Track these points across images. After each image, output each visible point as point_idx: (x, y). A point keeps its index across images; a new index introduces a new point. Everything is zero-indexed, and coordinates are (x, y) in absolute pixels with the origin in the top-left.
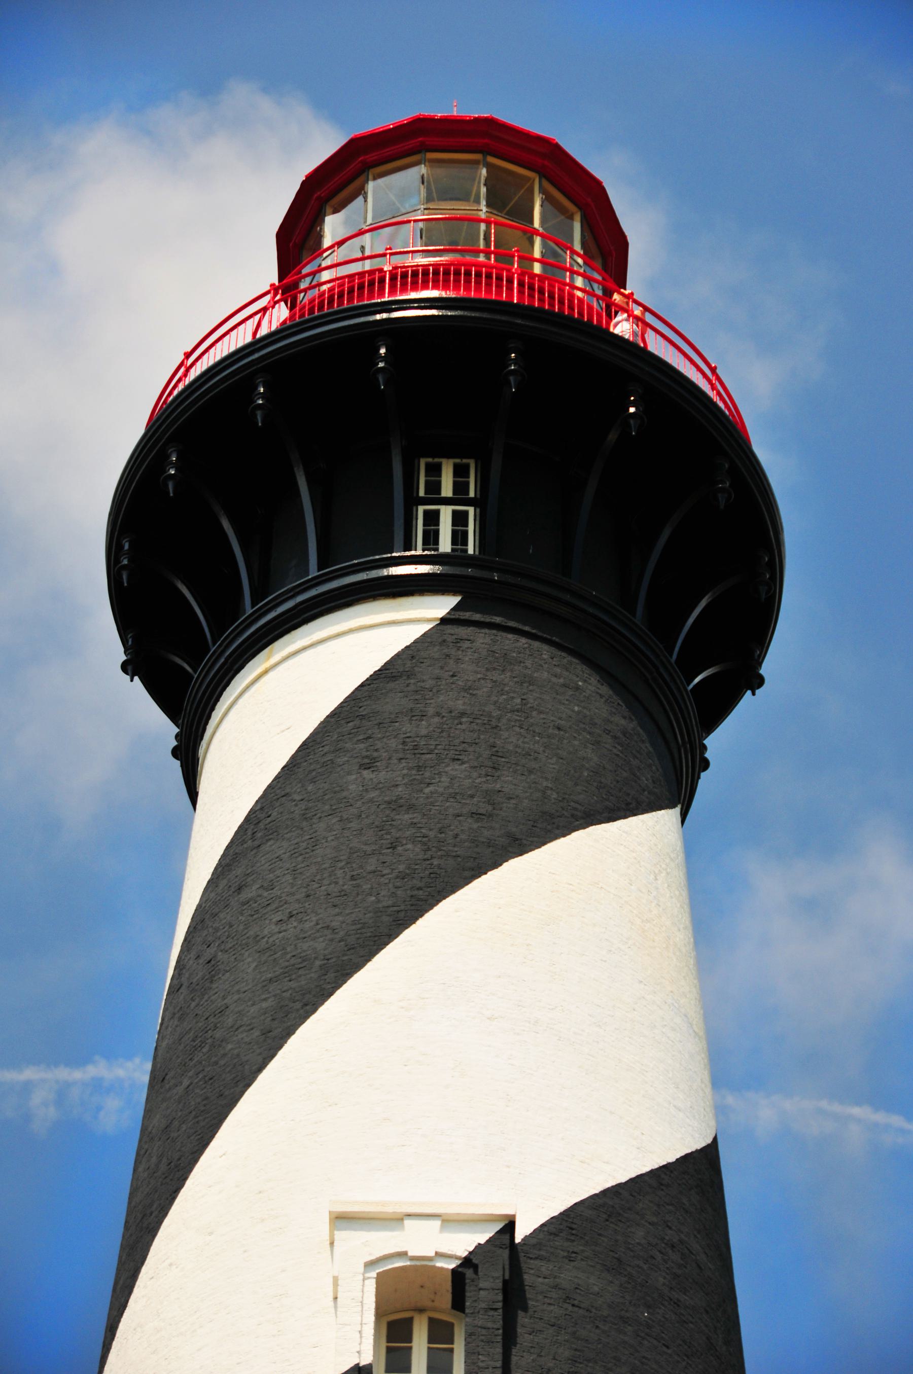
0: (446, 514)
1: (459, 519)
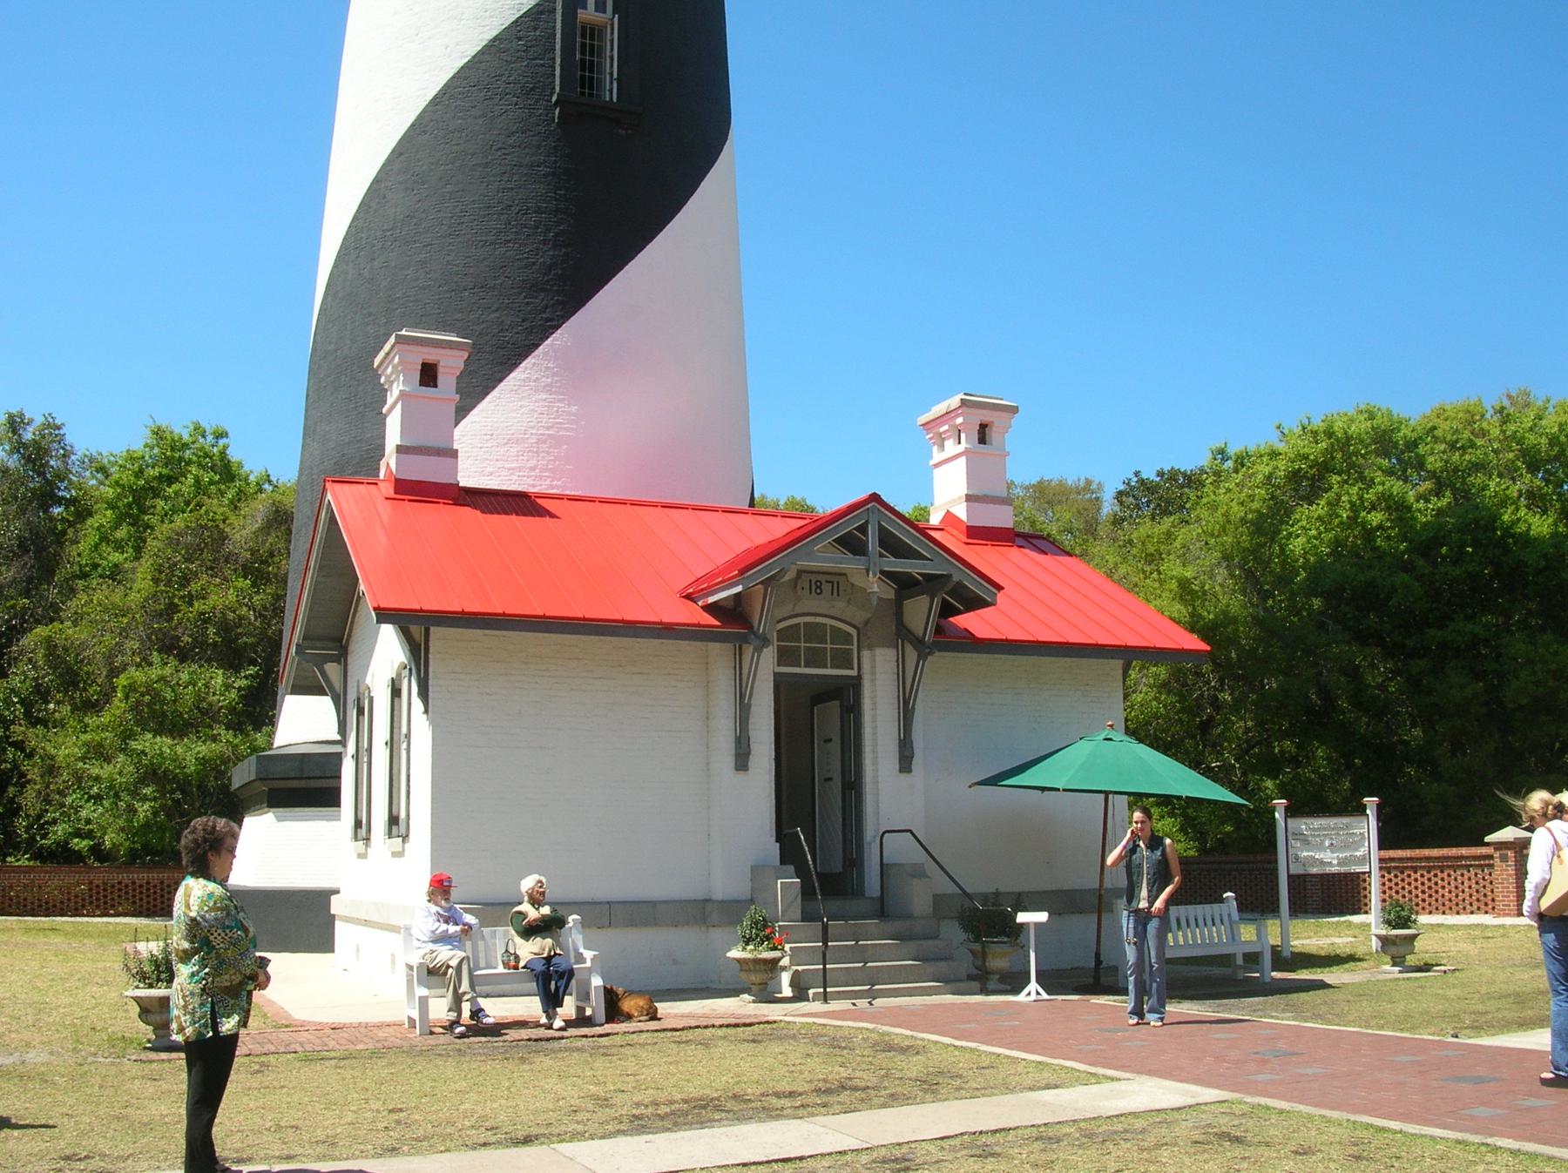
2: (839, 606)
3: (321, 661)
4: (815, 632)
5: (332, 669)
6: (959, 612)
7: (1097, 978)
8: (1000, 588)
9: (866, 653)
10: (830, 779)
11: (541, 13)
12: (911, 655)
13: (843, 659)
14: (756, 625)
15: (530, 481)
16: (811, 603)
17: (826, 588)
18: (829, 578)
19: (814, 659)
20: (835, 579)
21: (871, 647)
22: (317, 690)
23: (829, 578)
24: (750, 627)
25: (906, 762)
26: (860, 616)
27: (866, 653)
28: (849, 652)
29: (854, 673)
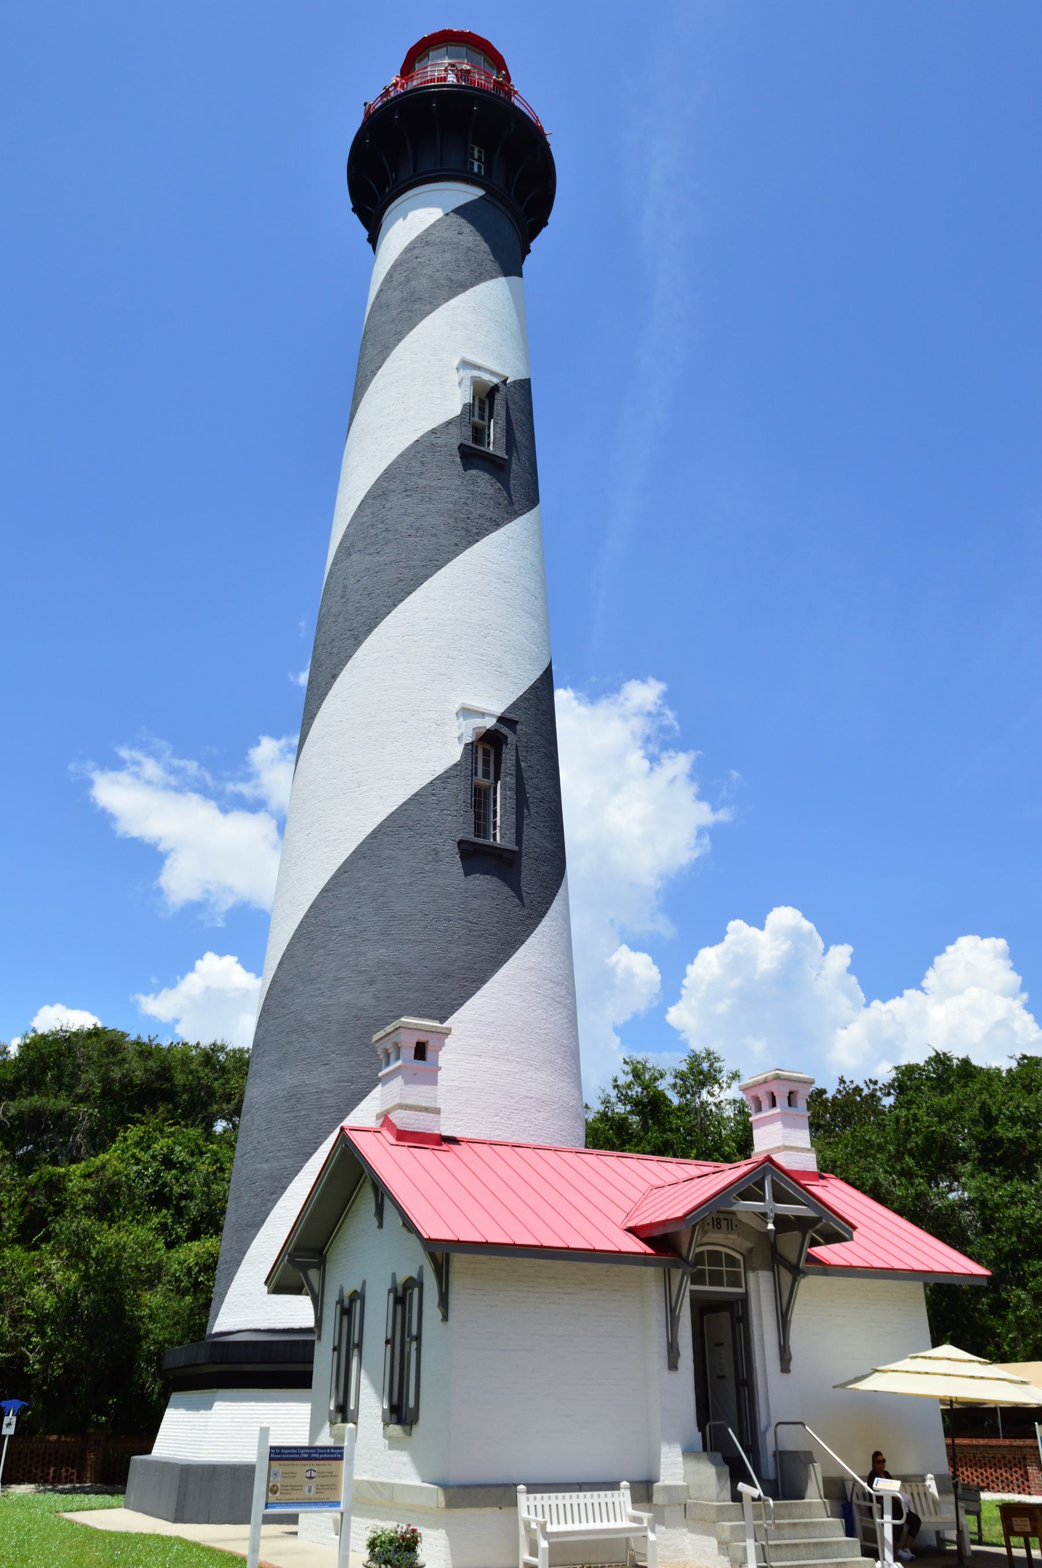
0: (476, 164)
1: (479, 167)
2: (733, 1238)
3: (304, 1268)
4: (715, 1257)
5: (313, 1274)
6: (819, 1244)
7: (980, 1537)
8: (854, 1228)
9: (751, 1275)
10: (724, 1377)
11: (449, 778)
12: (786, 1277)
13: (735, 1282)
14: (684, 1252)
15: (497, 1132)
16: (715, 1236)
17: (724, 1223)
18: (725, 1216)
19: (716, 1279)
20: (729, 1217)
21: (754, 1270)
22: (297, 1290)
23: (725, 1216)
24: (680, 1256)
25: (785, 1368)
26: (747, 1244)
27: (751, 1275)
28: (739, 1272)
29: (742, 1290)
